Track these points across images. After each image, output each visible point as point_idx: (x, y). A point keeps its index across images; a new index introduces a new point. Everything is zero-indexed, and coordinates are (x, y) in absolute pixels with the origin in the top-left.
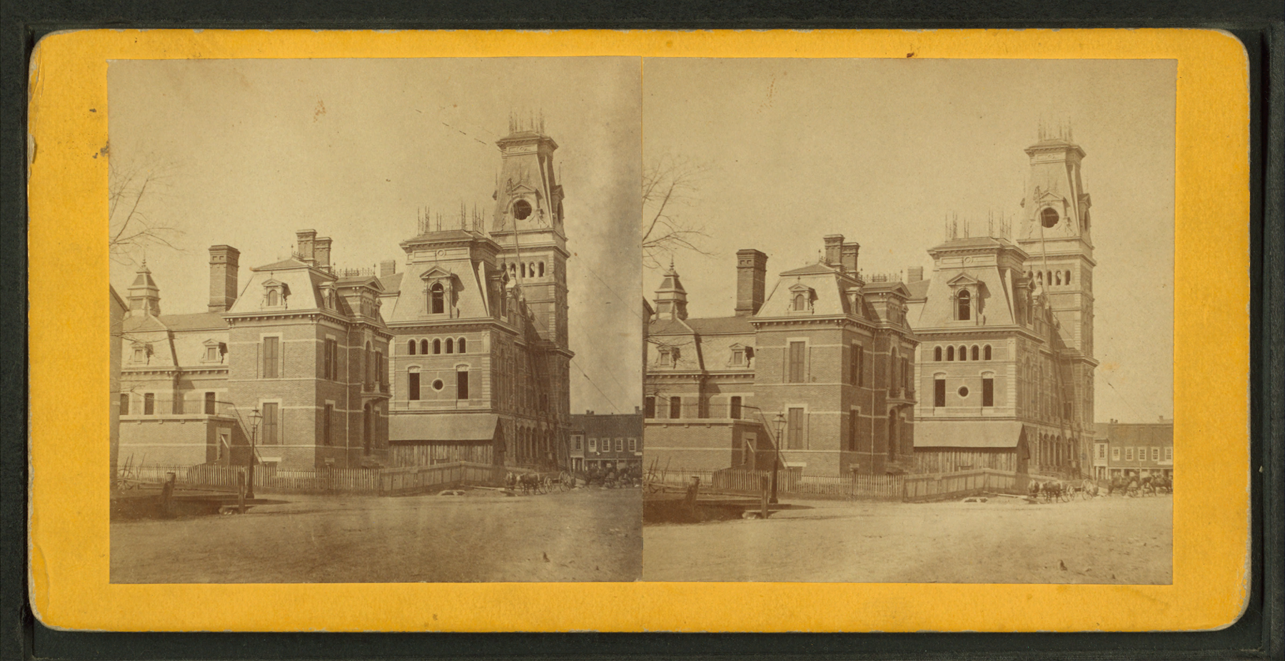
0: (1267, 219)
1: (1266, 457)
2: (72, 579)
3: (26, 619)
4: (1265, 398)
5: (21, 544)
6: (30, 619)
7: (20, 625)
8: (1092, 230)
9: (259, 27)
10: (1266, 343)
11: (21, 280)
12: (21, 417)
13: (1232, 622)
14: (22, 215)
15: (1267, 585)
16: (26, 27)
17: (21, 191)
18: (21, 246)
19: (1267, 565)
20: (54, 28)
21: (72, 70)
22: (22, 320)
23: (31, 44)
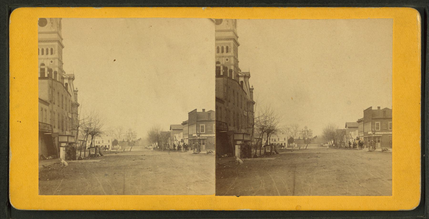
0: (426, 71)
1: (426, 151)
2: (25, 192)
3: (8, 206)
4: (426, 131)
5: (7, 181)
6: (10, 206)
7: (6, 208)
8: (63, 30)
9: (87, 6)
10: (426, 112)
11: (7, 92)
12: (7, 138)
13: (415, 208)
14: (7, 70)
15: (426, 194)
16: (8, 6)
17: (7, 44)
18: (7, 65)
19: (426, 188)
20: (18, 7)
21: (411, 18)
22: (7, 105)
23: (10, 12)
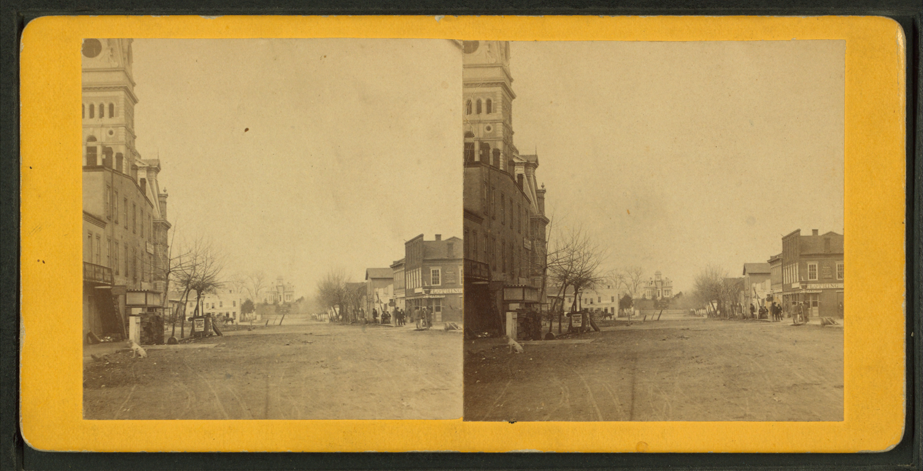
1: (916, 326)
2: (54, 412)
3: (18, 442)
6: (21, 442)
7: (13, 447)
11: (14, 197)
12: (14, 296)
13: (892, 447)
14: (15, 150)
16: (18, 14)
19: (917, 404)
20: (38, 14)
22: (15, 226)
23: (22, 26)
